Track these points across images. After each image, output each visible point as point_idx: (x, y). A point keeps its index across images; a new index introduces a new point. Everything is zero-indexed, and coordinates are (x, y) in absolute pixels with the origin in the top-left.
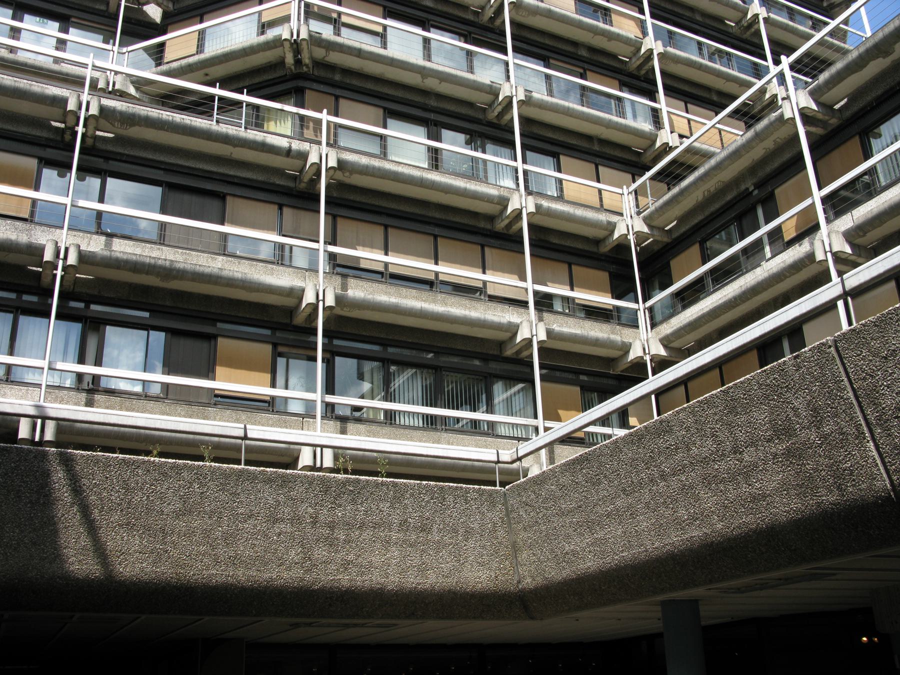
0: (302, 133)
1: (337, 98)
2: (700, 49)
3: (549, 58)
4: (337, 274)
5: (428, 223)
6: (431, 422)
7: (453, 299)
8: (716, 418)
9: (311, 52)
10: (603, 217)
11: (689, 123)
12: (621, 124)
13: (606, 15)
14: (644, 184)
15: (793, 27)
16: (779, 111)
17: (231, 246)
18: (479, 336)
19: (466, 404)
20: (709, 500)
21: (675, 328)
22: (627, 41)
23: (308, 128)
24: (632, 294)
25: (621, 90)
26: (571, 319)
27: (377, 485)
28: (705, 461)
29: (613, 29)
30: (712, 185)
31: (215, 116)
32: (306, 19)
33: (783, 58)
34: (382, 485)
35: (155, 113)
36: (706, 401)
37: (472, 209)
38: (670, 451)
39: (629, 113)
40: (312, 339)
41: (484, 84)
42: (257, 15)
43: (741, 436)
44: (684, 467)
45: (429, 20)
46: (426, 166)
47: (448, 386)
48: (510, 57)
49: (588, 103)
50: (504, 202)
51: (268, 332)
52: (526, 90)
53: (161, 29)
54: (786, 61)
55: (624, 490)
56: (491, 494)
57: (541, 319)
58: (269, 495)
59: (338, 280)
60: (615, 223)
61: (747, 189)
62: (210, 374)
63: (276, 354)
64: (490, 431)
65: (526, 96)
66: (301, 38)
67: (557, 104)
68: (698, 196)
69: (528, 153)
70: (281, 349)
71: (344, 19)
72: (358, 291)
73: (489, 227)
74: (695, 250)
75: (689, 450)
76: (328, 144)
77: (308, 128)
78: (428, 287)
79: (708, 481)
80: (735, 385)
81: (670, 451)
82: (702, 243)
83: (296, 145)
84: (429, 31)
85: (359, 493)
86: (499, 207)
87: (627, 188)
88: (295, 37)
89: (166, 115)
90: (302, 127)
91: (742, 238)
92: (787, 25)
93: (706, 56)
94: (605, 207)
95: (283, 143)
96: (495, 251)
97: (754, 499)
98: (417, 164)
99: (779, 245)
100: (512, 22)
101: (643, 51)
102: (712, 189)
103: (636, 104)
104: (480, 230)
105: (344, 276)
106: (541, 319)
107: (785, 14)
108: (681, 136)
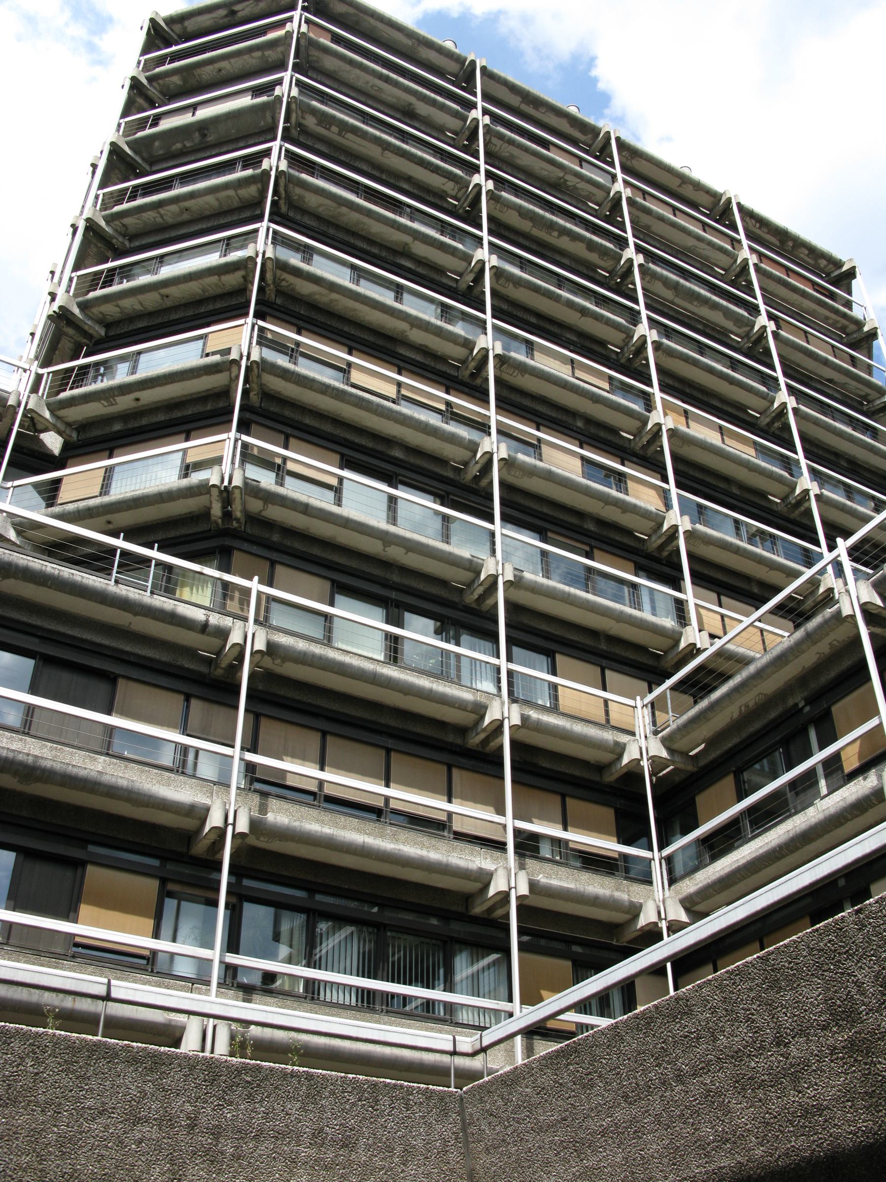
0: (224, 605)
1: (273, 563)
2: (737, 529)
3: (546, 530)
4: (256, 791)
5: (380, 733)
6: (368, 1002)
7: (404, 834)
8: (752, 995)
9: (244, 504)
10: (608, 736)
11: (723, 620)
12: (636, 618)
13: (620, 481)
14: (663, 695)
15: (851, 508)
16: (836, 607)
17: (117, 745)
18: (440, 885)
19: (417, 981)
20: (744, 1114)
21: (701, 885)
22: (645, 514)
23: (232, 599)
24: (644, 840)
25: (636, 575)
26: (563, 869)
27: (285, 1075)
28: (737, 1056)
29: (628, 498)
30: (750, 698)
31: (114, 574)
32: (243, 462)
33: (839, 540)
34: (292, 1076)
35: (38, 564)
36: (739, 972)
37: (438, 716)
38: (690, 1041)
39: (647, 605)
40: (214, 876)
41: (461, 558)
42: (181, 453)
43: (786, 1020)
44: (709, 1063)
45: (397, 475)
46: (382, 658)
47: (393, 955)
48: (497, 526)
49: (594, 588)
50: (480, 710)
51: (155, 862)
52: (515, 569)
53: (59, 463)
54: (843, 545)
55: (626, 1097)
56: (442, 1097)
57: (522, 867)
58: (131, 1082)
59: (256, 799)
60: (625, 745)
61: (796, 705)
62: (72, 915)
63: (165, 893)
64: (448, 1017)
65: (515, 576)
66: (234, 484)
67: (555, 588)
68: (732, 712)
69: (515, 650)
70: (171, 887)
71: (290, 466)
72: (281, 815)
73: (459, 741)
74: (728, 782)
75: (715, 1039)
76: (256, 621)
77: (232, 599)
78: (374, 817)
79: (741, 1084)
80: (778, 948)
81: (690, 1041)
82: (738, 773)
83: (215, 619)
84: (396, 488)
85: (258, 1086)
86: (473, 717)
87: (642, 699)
88: (226, 483)
89: (52, 568)
90: (225, 596)
91: (790, 767)
92: (845, 505)
93: (744, 535)
94: (612, 723)
95: (199, 615)
96: (465, 774)
97: (806, 1113)
98: (370, 655)
99: (837, 777)
100: (502, 483)
101: (666, 527)
102: (751, 704)
103: (656, 593)
104: (451, 747)
105: (264, 795)
106: (522, 867)
107: (842, 492)
108: (712, 636)
